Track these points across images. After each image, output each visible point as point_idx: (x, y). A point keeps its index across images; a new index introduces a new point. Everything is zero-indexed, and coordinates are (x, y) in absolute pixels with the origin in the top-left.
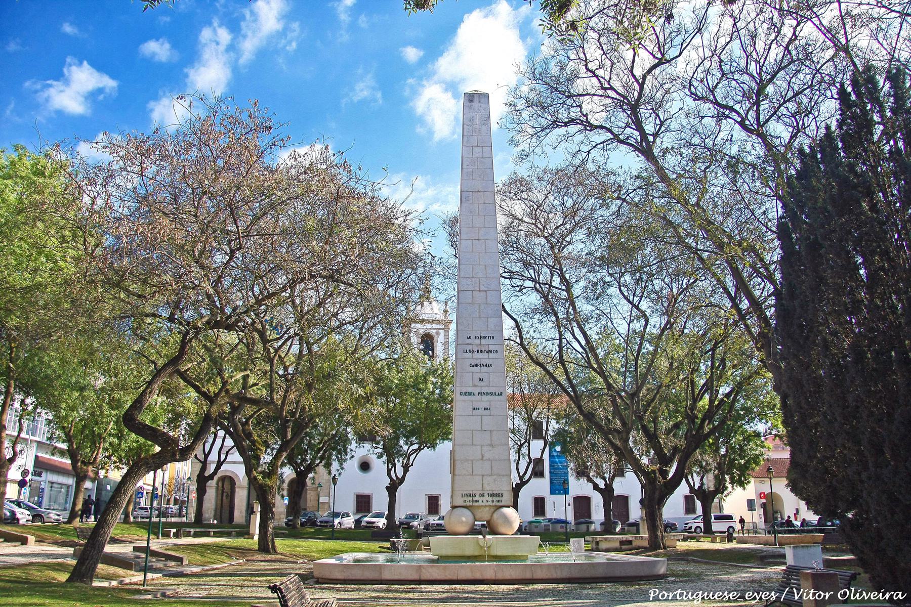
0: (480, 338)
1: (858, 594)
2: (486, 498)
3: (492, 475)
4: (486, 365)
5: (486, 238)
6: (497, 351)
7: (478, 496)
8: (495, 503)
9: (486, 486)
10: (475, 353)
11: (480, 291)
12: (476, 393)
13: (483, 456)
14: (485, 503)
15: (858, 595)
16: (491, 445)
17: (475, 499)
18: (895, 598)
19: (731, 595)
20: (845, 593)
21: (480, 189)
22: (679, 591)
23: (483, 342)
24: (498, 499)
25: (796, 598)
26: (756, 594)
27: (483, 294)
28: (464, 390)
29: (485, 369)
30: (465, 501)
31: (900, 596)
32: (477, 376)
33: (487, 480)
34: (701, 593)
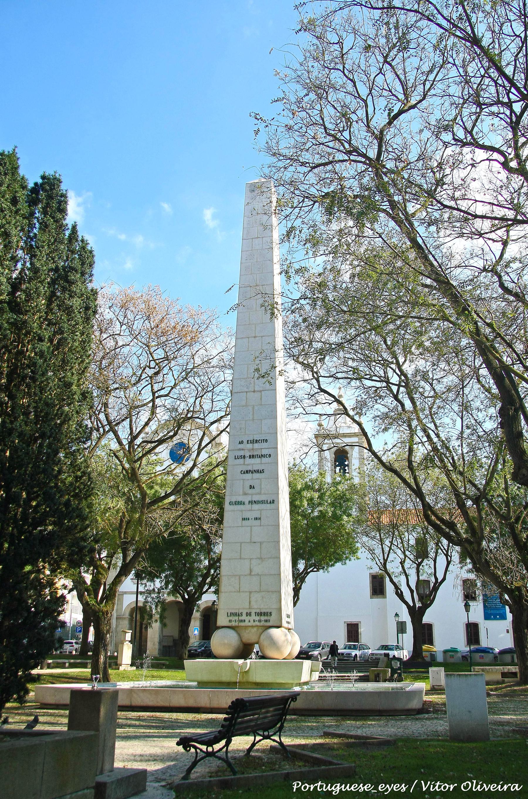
0: (253, 442)
1: (479, 786)
2: (253, 617)
4: (257, 471)
5: (262, 334)
6: (270, 456)
8: (262, 623)
9: (253, 603)
10: (247, 459)
11: (254, 391)
12: (247, 502)
13: (251, 571)
14: (252, 623)
15: (479, 786)
16: (261, 558)
17: (241, 618)
18: (512, 790)
19: (366, 787)
20: (468, 784)
21: (258, 283)
22: (320, 783)
23: (256, 446)
24: (266, 618)
25: (424, 789)
26: (388, 786)
27: (257, 395)
28: (234, 500)
30: (230, 621)
31: (516, 787)
33: (255, 597)
34: (339, 785)
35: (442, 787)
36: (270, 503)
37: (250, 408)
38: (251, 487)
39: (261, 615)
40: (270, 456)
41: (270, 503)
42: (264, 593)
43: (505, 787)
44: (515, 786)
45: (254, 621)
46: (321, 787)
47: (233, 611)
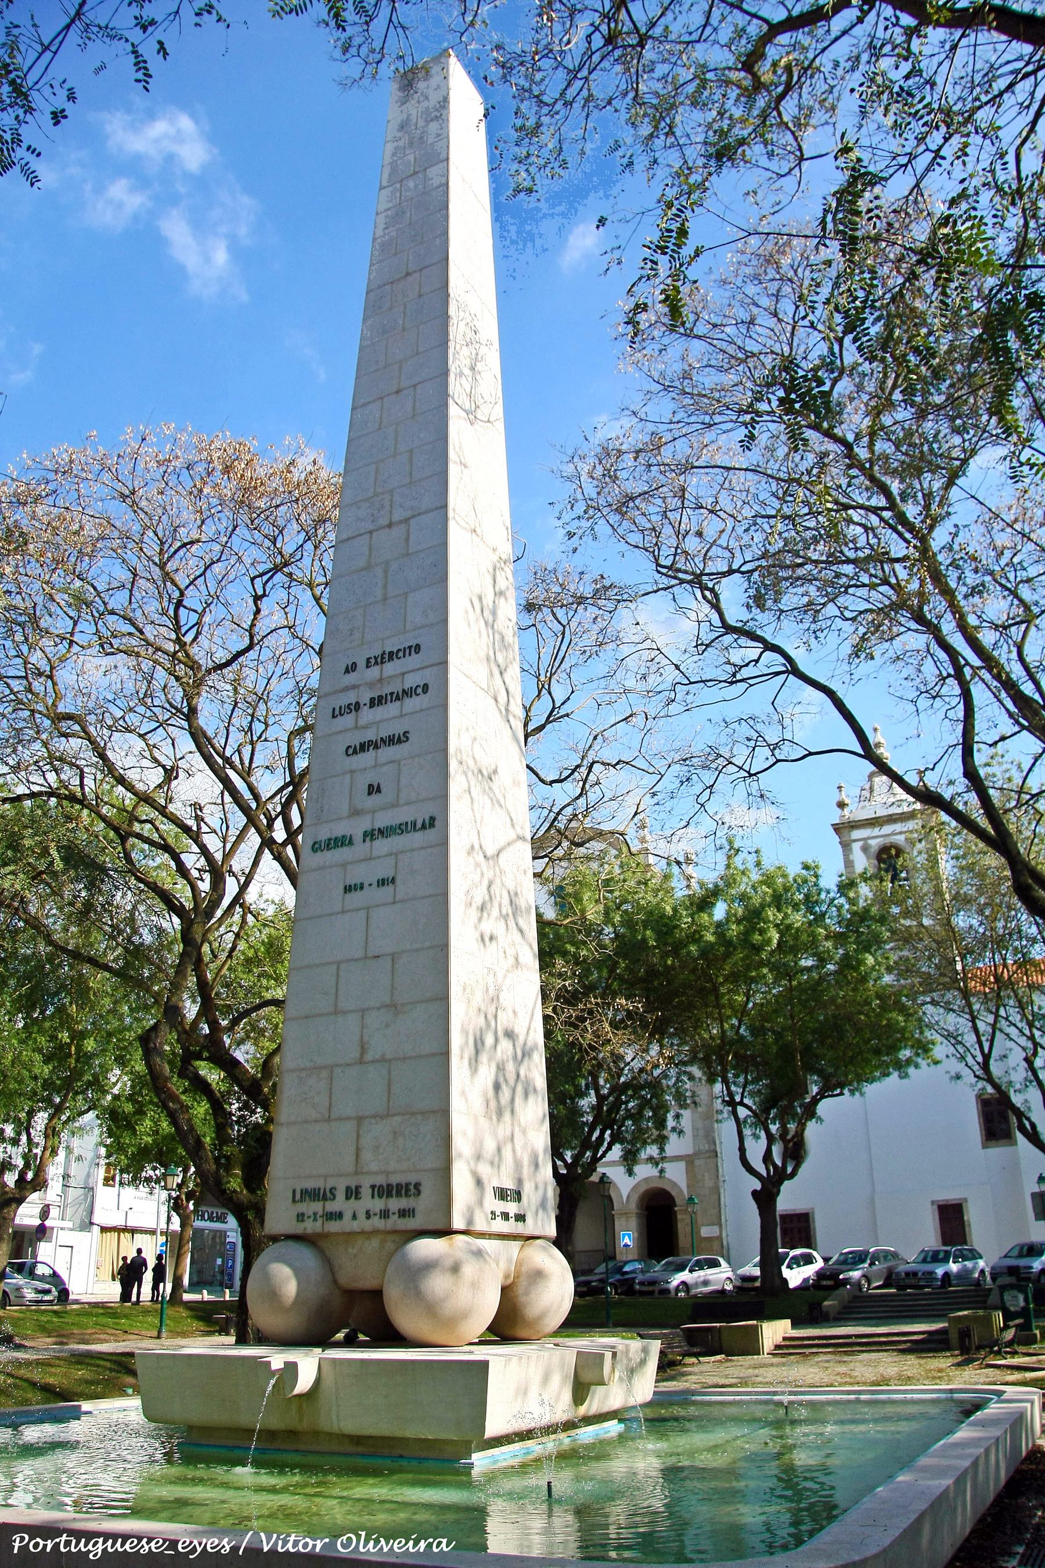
3: (388, 1115)
4: (392, 741)
7: (341, 1195)
8: (395, 1222)
9: (367, 1155)
12: (358, 837)
13: (363, 1048)
14: (362, 1224)
17: (332, 1206)
19: (153, 1545)
20: (349, 1539)
22: (64, 1537)
23: (390, 668)
24: (403, 1203)
29: (387, 753)
30: (301, 1217)
31: (444, 1545)
32: (363, 782)
33: (378, 1131)
34: (101, 1540)
35: (301, 1544)
36: (424, 827)
37: (379, 571)
38: (373, 789)
39: (389, 1195)
40: (426, 688)
41: (424, 827)
42: (398, 1119)
43: (422, 1545)
44: (440, 1543)
45: (368, 1215)
46: (68, 1543)
47: (310, 1184)
